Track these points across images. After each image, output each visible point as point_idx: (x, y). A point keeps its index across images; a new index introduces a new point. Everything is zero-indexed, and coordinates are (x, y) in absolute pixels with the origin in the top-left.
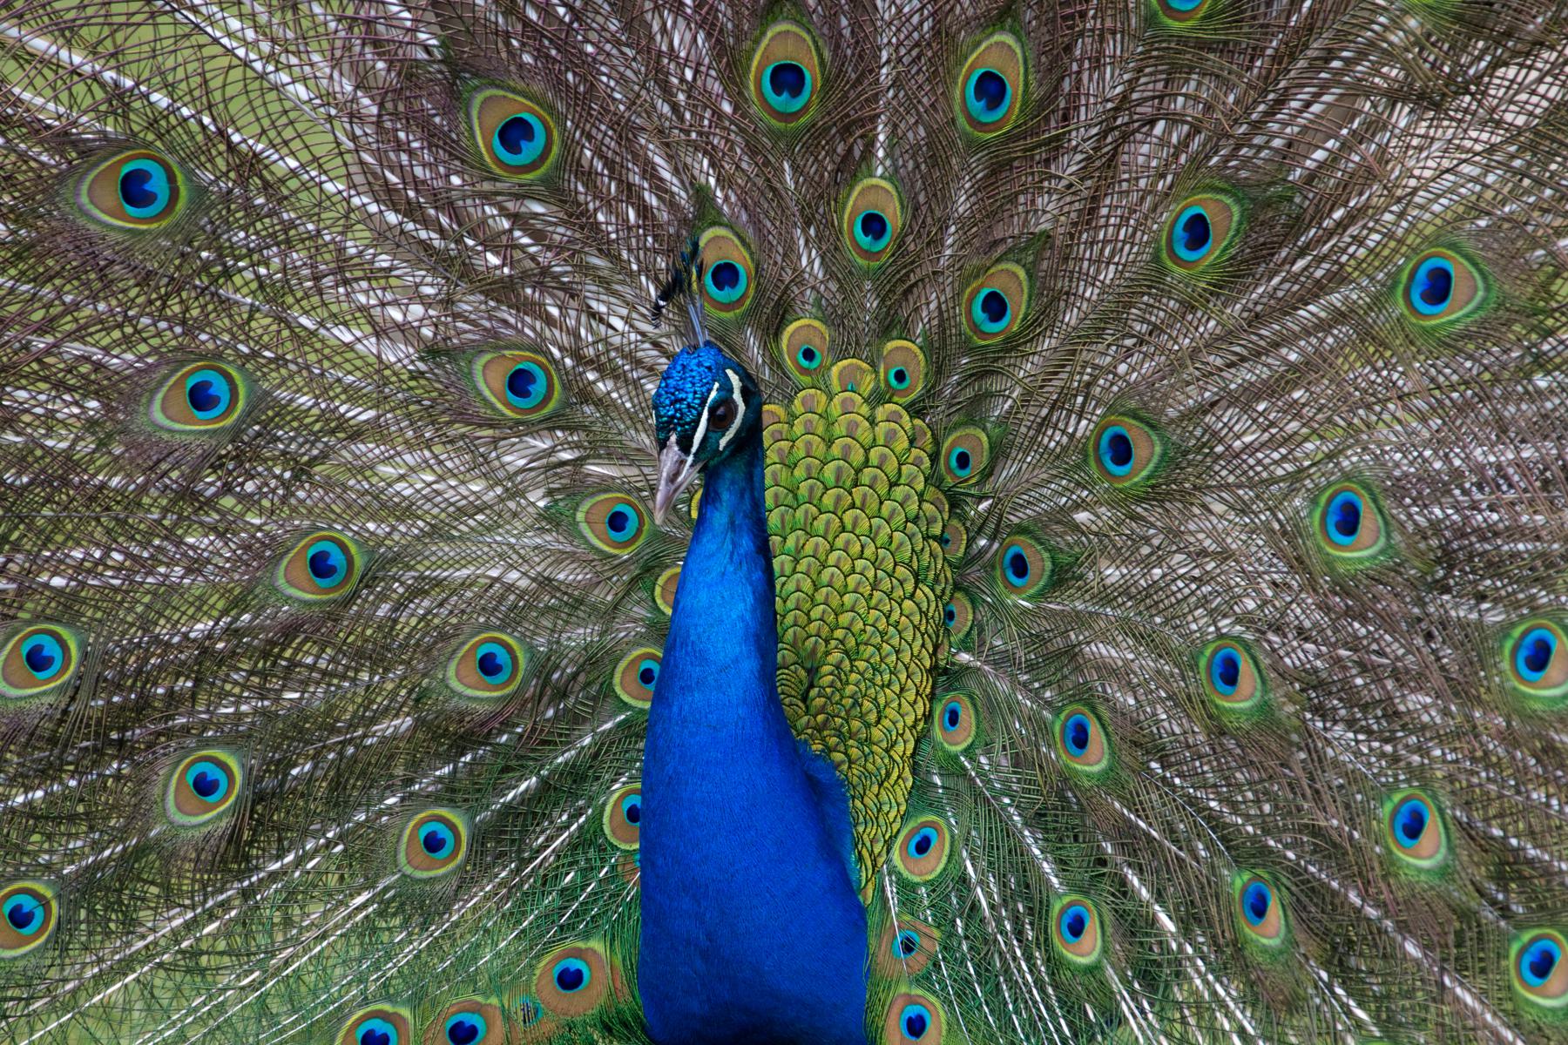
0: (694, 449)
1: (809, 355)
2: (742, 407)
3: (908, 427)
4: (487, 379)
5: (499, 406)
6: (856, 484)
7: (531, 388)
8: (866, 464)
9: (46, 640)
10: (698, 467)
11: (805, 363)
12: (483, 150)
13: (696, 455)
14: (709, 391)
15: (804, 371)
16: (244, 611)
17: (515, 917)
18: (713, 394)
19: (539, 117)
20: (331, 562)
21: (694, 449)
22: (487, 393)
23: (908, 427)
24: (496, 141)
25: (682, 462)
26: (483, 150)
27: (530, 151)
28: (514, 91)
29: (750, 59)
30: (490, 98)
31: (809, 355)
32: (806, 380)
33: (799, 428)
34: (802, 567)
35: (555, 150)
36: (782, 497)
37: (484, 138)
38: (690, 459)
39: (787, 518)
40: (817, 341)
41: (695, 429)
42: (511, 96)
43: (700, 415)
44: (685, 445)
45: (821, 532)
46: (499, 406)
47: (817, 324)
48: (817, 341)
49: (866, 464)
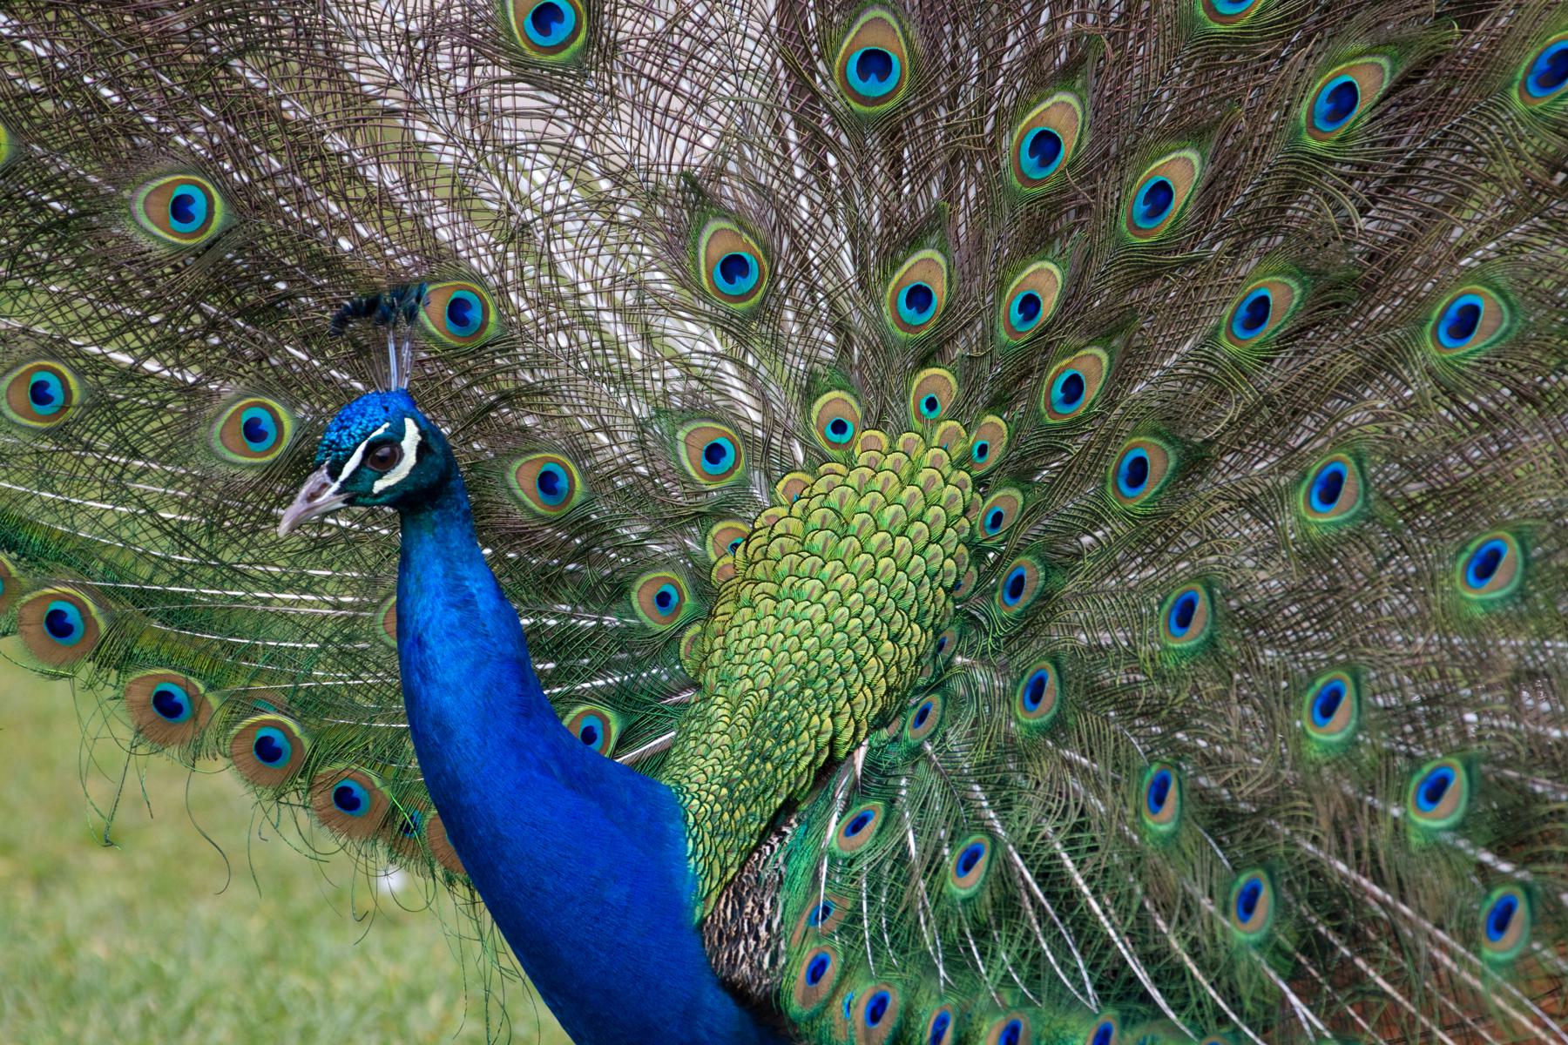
0: (342, 477)
1: (932, 404)
2: (410, 459)
3: (968, 497)
4: (714, 240)
5: (703, 269)
6: (902, 534)
7: (738, 279)
8: (920, 518)
9: (887, 87)
10: (343, 497)
11: (925, 410)
12: (842, 52)
13: (343, 483)
14: (376, 428)
15: (919, 415)
16: (156, 311)
17: (1044, 838)
18: (380, 432)
19: (902, 71)
20: (468, 314)
21: (342, 477)
22: (702, 252)
23: (968, 497)
24: (857, 56)
25: (325, 486)
26: (842, 52)
27: (873, 87)
28: (904, 33)
29: (1153, 161)
30: (883, 20)
31: (932, 404)
32: (918, 425)
33: (888, 463)
34: (826, 598)
35: (890, 105)
36: (829, 521)
37: (851, 44)
38: (336, 486)
39: (831, 543)
40: (945, 395)
41: (348, 458)
42: (899, 34)
43: (357, 445)
44: (334, 473)
45: (856, 571)
46: (703, 269)
47: (952, 380)
48: (945, 395)
49: (920, 518)
